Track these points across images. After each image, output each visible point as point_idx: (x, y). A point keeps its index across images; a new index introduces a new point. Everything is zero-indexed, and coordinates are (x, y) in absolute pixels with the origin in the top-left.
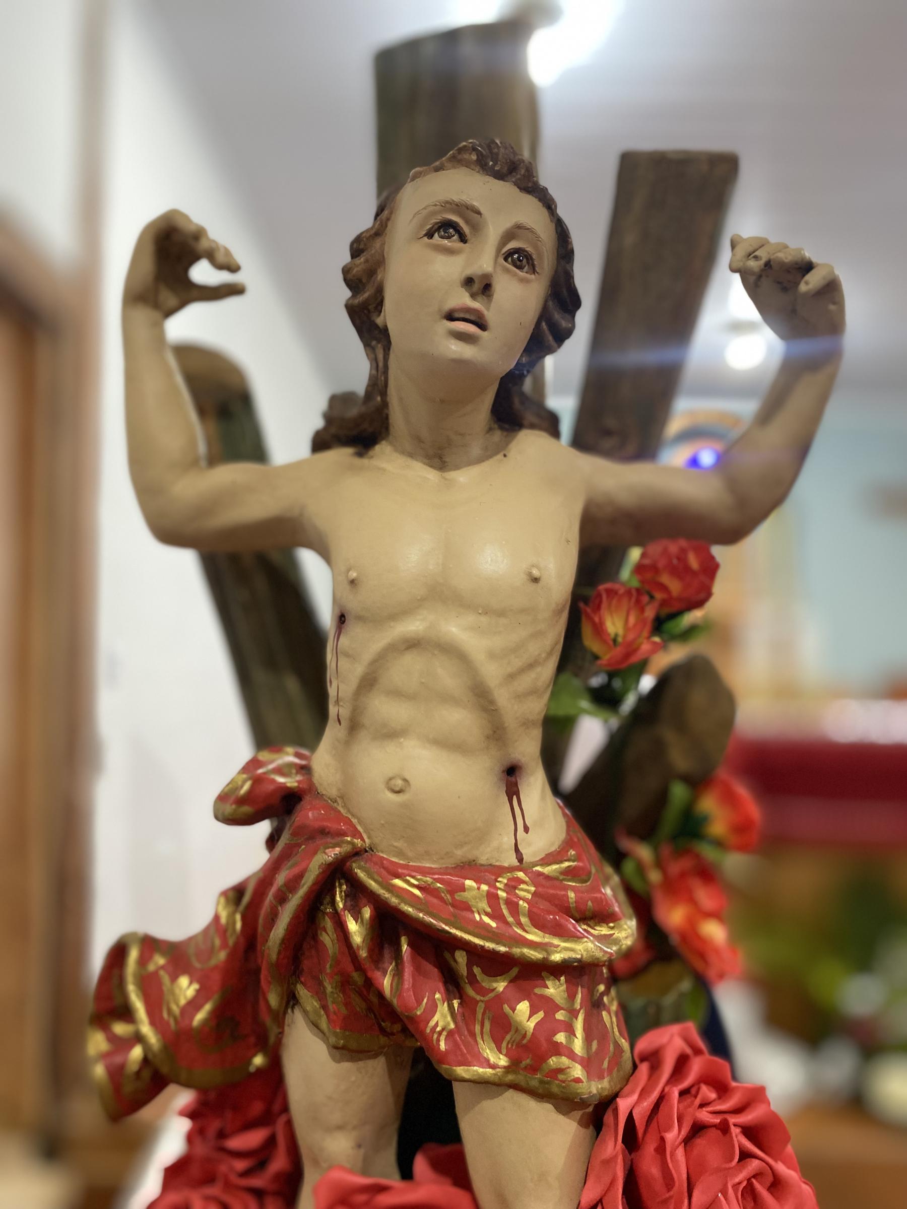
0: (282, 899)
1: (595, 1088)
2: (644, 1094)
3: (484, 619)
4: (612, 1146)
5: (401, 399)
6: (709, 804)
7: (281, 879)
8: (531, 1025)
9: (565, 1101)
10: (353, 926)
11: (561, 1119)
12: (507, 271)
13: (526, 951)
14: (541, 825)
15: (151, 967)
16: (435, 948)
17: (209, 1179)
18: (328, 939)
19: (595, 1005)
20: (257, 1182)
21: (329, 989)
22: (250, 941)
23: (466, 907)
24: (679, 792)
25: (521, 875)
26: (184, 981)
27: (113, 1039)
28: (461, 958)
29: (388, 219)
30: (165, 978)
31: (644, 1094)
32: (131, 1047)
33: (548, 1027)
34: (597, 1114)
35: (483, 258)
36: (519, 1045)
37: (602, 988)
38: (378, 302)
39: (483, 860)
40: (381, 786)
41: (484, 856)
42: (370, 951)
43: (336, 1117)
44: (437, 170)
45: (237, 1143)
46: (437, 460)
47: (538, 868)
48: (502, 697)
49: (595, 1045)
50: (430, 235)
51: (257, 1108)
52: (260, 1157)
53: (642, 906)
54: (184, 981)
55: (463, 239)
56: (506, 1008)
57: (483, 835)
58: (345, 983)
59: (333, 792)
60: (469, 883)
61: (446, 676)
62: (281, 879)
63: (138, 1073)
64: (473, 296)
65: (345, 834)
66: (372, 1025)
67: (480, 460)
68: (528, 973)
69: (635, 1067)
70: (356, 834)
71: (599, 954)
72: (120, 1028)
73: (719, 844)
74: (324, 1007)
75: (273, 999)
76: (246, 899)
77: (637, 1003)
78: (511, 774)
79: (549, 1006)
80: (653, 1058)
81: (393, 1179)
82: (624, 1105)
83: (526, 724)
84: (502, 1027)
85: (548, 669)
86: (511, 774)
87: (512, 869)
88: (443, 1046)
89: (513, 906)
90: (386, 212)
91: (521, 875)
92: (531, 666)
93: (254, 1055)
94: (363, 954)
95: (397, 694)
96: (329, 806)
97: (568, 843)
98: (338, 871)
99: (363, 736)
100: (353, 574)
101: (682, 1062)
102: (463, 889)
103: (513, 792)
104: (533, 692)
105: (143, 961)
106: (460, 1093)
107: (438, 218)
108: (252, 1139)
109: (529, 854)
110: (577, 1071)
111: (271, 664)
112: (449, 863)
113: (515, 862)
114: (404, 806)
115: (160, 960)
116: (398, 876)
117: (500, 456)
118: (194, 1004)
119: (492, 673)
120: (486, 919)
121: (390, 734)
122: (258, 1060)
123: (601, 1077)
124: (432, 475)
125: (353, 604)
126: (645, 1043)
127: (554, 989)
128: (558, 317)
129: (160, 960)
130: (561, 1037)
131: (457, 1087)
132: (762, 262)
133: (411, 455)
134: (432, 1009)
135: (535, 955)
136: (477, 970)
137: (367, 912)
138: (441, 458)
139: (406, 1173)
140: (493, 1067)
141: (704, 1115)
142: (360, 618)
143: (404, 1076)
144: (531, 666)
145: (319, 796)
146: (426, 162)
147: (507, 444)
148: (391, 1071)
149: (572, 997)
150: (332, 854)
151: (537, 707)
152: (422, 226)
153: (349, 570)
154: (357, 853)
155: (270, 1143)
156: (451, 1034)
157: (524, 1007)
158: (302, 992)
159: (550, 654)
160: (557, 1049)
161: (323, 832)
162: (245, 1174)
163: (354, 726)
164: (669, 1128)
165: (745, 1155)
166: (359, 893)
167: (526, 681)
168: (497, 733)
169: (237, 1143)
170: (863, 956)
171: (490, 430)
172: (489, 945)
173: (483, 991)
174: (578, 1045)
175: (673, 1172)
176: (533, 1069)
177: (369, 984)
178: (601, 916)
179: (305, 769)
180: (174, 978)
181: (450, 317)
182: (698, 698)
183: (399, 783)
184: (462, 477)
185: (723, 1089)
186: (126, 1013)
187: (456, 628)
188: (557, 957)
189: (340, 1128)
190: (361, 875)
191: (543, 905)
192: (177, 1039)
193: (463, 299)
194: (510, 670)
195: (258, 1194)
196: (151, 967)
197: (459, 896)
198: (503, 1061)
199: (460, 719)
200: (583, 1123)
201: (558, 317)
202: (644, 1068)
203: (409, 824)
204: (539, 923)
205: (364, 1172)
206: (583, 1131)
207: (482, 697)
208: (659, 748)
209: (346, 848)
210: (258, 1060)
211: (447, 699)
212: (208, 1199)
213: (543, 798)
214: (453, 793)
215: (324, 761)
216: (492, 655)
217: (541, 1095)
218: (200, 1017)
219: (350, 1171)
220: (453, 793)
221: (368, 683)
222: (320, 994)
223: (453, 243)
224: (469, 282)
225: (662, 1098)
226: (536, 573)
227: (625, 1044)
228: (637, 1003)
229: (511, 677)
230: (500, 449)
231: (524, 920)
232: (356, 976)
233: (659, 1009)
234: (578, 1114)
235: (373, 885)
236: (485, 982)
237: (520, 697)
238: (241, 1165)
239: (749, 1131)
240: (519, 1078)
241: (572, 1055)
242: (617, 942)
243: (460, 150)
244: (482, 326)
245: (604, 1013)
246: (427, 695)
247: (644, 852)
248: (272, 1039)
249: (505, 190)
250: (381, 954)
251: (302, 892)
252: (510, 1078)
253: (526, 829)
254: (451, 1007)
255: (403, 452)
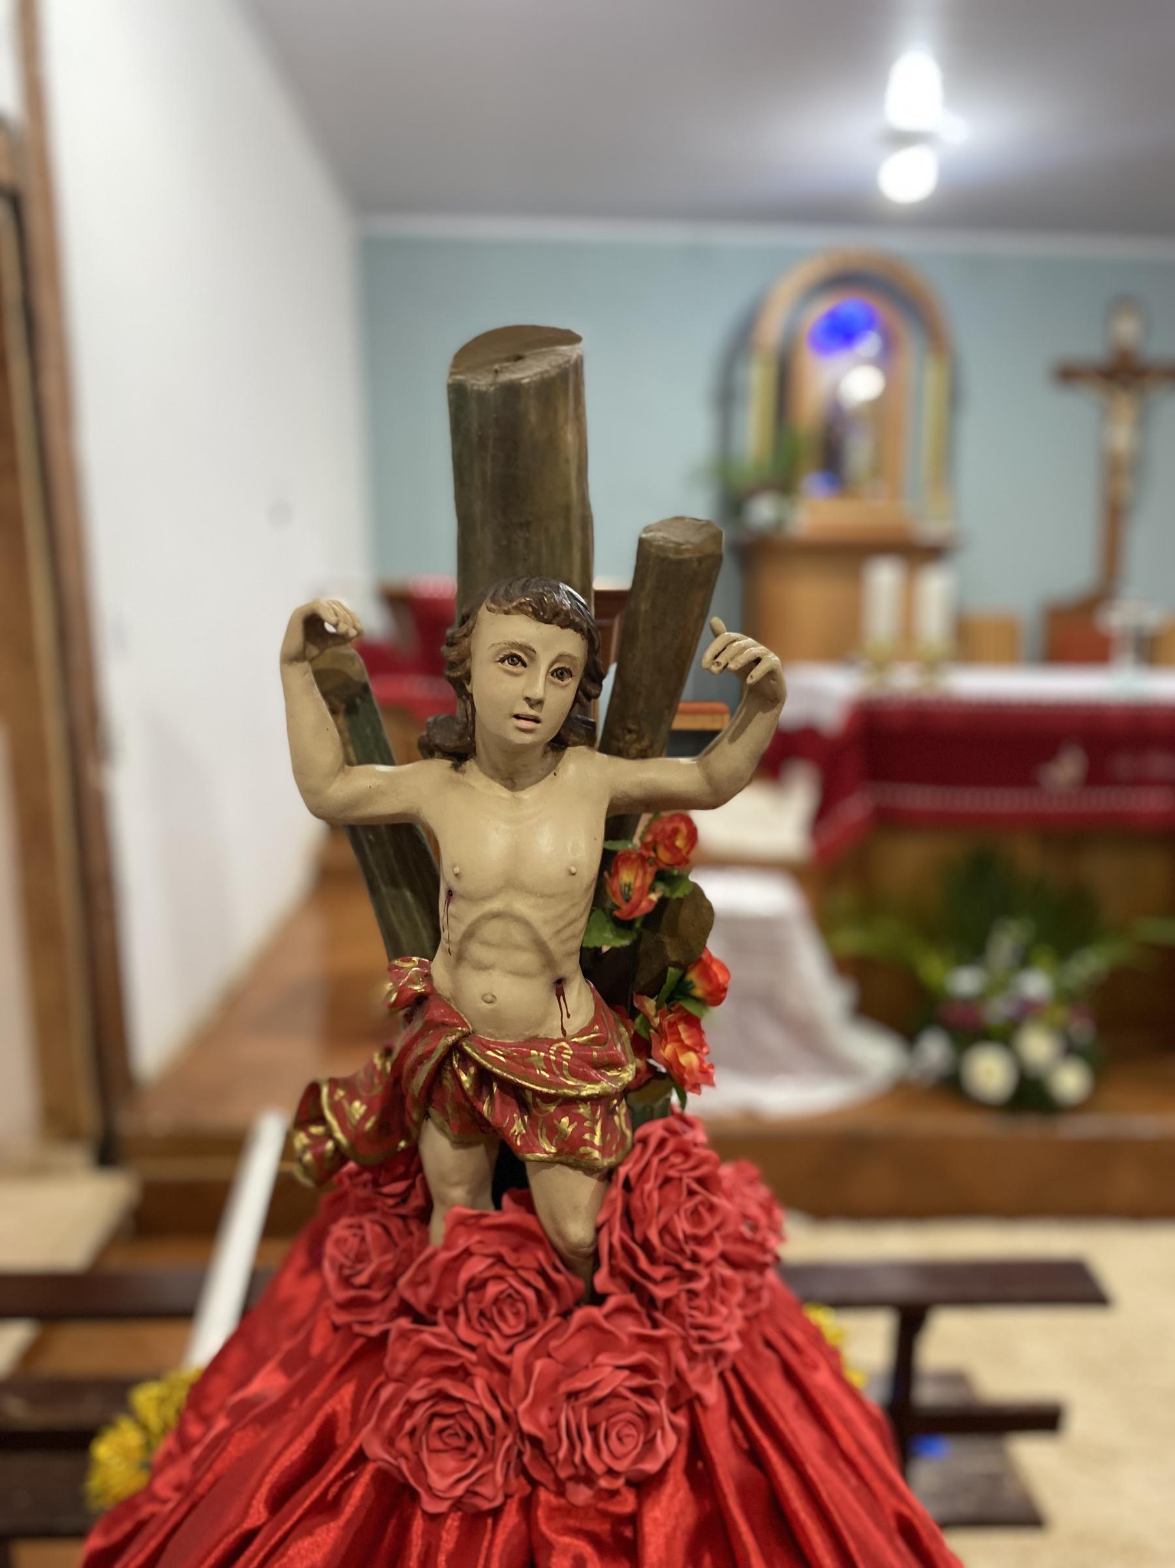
0: (420, 1061)
1: (606, 1162)
2: (636, 1162)
3: (541, 901)
4: (616, 1192)
5: (484, 745)
6: (692, 976)
7: (419, 1050)
8: (570, 1130)
9: (590, 1170)
10: (464, 1078)
11: (589, 1178)
12: (554, 683)
13: (566, 1091)
14: (581, 1000)
15: (336, 1098)
16: (515, 1092)
17: (373, 1209)
18: (448, 1082)
19: (610, 1112)
20: (402, 1211)
21: (450, 1112)
22: (396, 1081)
23: (532, 1066)
24: (671, 970)
25: (564, 1044)
26: (357, 1104)
27: (310, 1136)
28: (529, 1094)
29: (473, 627)
30: (346, 1104)
31: (636, 1162)
32: (325, 1142)
33: (579, 1131)
34: (608, 1175)
35: (537, 683)
36: (563, 1141)
37: (615, 1102)
38: (468, 677)
39: (542, 1035)
40: (479, 999)
41: (542, 1034)
42: (475, 1091)
43: (455, 1178)
44: (507, 613)
45: (387, 1189)
46: (509, 782)
47: (576, 1040)
48: (553, 945)
49: (608, 1137)
50: (502, 661)
51: (401, 1169)
52: (404, 1197)
53: (642, 1047)
54: (357, 1104)
55: (524, 665)
56: (555, 1122)
57: (540, 1023)
58: (459, 1108)
59: (447, 994)
60: (533, 1052)
61: (518, 935)
62: (419, 1050)
63: (332, 1158)
64: (531, 706)
65: (457, 1025)
66: (472, 1129)
67: (537, 781)
68: (569, 1103)
69: (633, 1146)
70: (464, 1024)
71: (609, 1090)
72: (316, 1130)
73: (697, 1000)
74: (448, 1121)
75: (415, 1116)
76: (395, 1055)
77: (639, 1106)
78: (559, 986)
79: (580, 1119)
80: (644, 1141)
81: (491, 1210)
82: (622, 1171)
83: (569, 954)
84: (553, 1132)
85: (581, 924)
86: (559, 986)
87: (559, 1041)
88: (518, 1143)
89: (559, 1065)
90: (471, 622)
91: (564, 1044)
92: (570, 924)
93: (400, 1140)
94: (471, 1093)
95: (487, 944)
96: (444, 1003)
97: (594, 1021)
98: (456, 1047)
99: (465, 963)
100: (457, 870)
101: (662, 1143)
102: (529, 1055)
103: (560, 993)
104: (574, 937)
105: (331, 1094)
106: (530, 1168)
107: (507, 652)
108: (399, 1187)
109: (570, 1031)
110: (596, 1154)
111: (395, 884)
112: (521, 1039)
113: (562, 1036)
114: (493, 1010)
115: (341, 1093)
116: (490, 1049)
117: (552, 775)
118: (365, 1118)
119: (546, 932)
120: (543, 1073)
121: (482, 967)
122: (402, 1144)
123: (610, 1156)
124: (505, 793)
125: (457, 887)
126: (640, 1132)
127: (583, 1110)
128: (591, 688)
129: (341, 1093)
130: (587, 1136)
131: (528, 1165)
132: (721, 668)
133: (492, 777)
134: (512, 1123)
135: (573, 1093)
136: (538, 1100)
137: (472, 1070)
138: (511, 779)
139: (498, 1206)
140: (546, 1152)
141: (672, 1173)
142: (462, 897)
143: (495, 1153)
144: (570, 924)
145: (439, 995)
146: (503, 779)
147: (558, 762)
148: (488, 1151)
149: (594, 1113)
150: (451, 1039)
151: (575, 944)
152: (497, 654)
153: (454, 866)
154: (465, 1036)
155: (412, 1187)
156: (523, 1136)
157: (565, 1120)
158: (432, 1111)
159: (582, 915)
160: (585, 1143)
161: (444, 1024)
162: (396, 1206)
163: (460, 958)
164: (647, 1181)
165: (691, 1193)
166: (466, 1059)
167: (568, 933)
168: (549, 962)
169: (387, 1189)
170: (972, 950)
171: (545, 753)
172: (545, 1090)
173: (540, 1111)
174: (597, 1140)
175: (222, 1546)
176: (571, 1153)
177: (474, 1108)
178: (616, 1064)
179: (428, 977)
180: (351, 1102)
181: (517, 717)
182: (686, 913)
183: (489, 998)
184: (527, 795)
185: (687, 1154)
186: (321, 1120)
187: (522, 906)
188: (584, 1093)
189: (457, 1184)
190: (469, 1049)
191: (578, 1062)
192: (357, 1136)
193: (526, 710)
194: (558, 928)
195: (404, 1218)
196: (336, 1098)
197: (527, 1060)
198: (553, 1150)
199: (528, 959)
200: (600, 1179)
201: (591, 688)
202: (639, 1147)
203: (497, 1020)
204: (574, 1074)
205: (472, 1207)
206: (602, 1184)
207: (540, 946)
208: (660, 945)
209: (458, 1034)
210: (402, 1144)
211: (518, 947)
212: (373, 1222)
213: (579, 993)
214: (511, 988)
215: (439, 968)
216: (546, 922)
217: (574, 1166)
218: (369, 1125)
219: (465, 1206)
220: (511, 988)
221: (469, 935)
222: (444, 1112)
223: (519, 669)
224: (527, 699)
225: (648, 1164)
226: (573, 870)
227: (628, 1133)
228: (639, 1106)
229: (558, 932)
230: (552, 769)
231: (565, 1072)
232: (467, 1105)
233: (652, 1110)
234: (598, 1175)
235: (477, 1057)
236: (543, 1107)
237: (563, 942)
238: (391, 1202)
239: (700, 1181)
240: (563, 1158)
241: (593, 1145)
242: (622, 1079)
243: (521, 604)
244: (536, 720)
245: (616, 1118)
246: (505, 945)
247: (650, 1005)
248: (414, 1136)
249: (552, 630)
250: (481, 1092)
251: (433, 1061)
252: (557, 1158)
253: (568, 1016)
254: (523, 1121)
255: (485, 773)
